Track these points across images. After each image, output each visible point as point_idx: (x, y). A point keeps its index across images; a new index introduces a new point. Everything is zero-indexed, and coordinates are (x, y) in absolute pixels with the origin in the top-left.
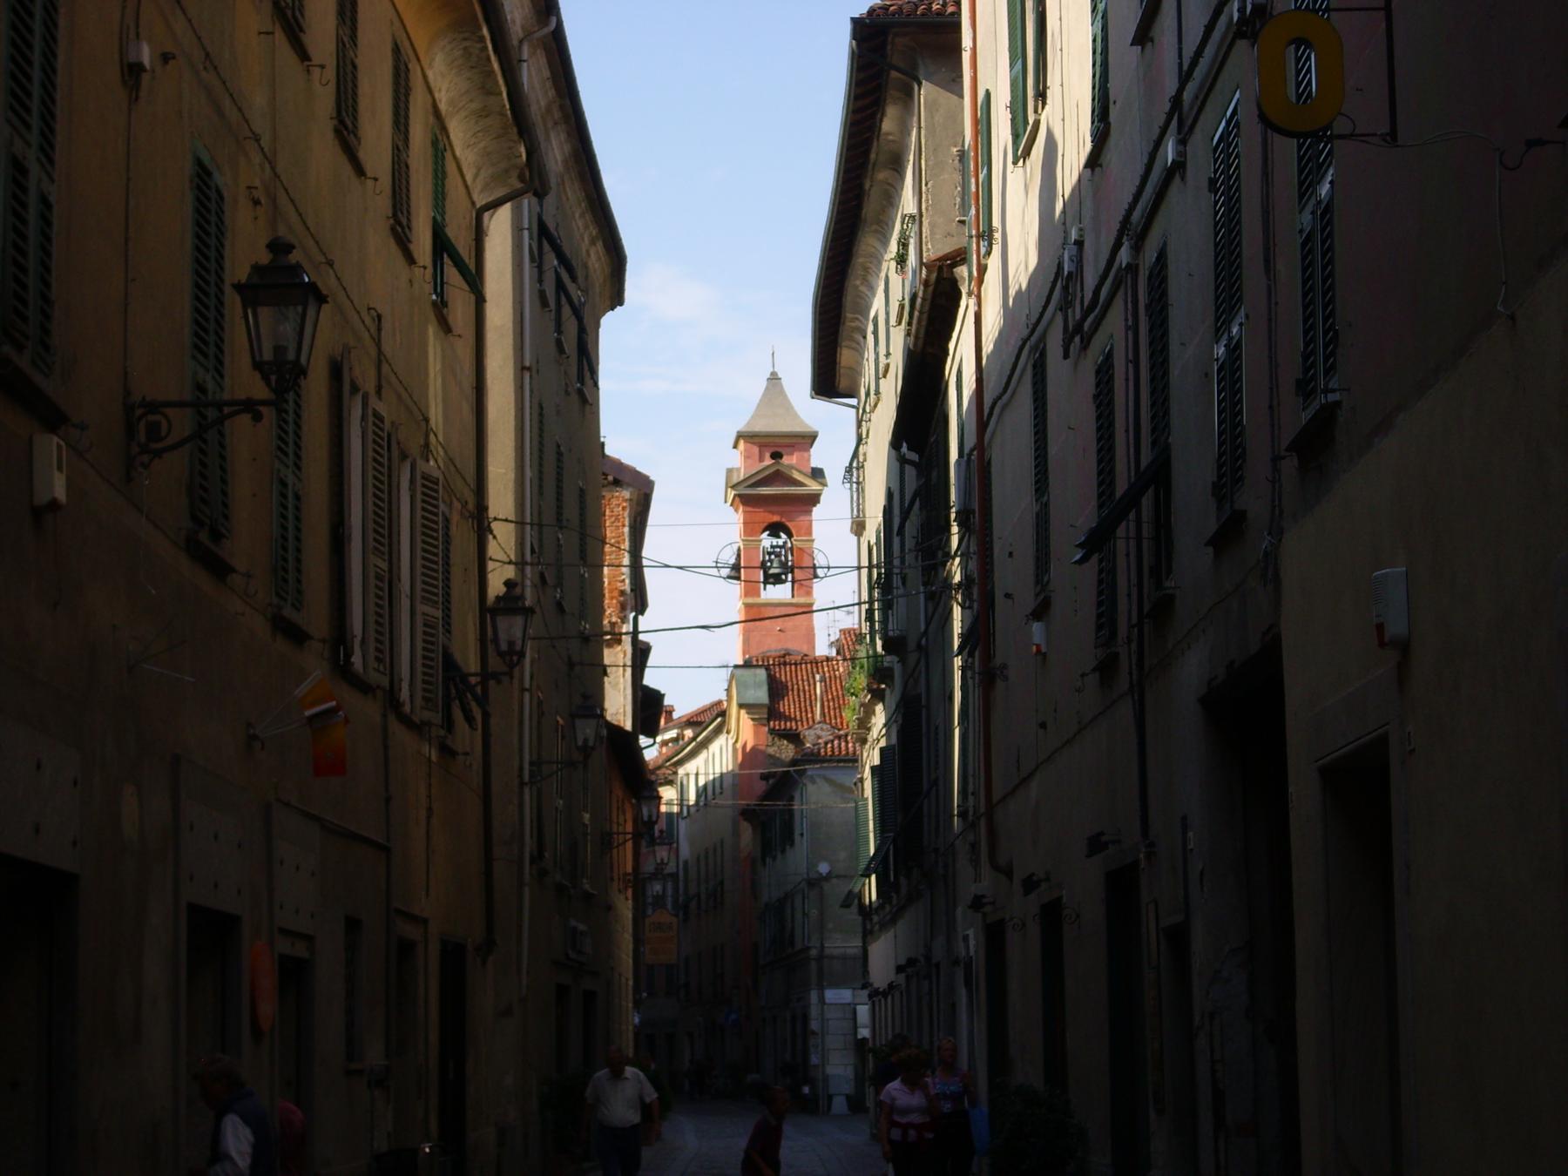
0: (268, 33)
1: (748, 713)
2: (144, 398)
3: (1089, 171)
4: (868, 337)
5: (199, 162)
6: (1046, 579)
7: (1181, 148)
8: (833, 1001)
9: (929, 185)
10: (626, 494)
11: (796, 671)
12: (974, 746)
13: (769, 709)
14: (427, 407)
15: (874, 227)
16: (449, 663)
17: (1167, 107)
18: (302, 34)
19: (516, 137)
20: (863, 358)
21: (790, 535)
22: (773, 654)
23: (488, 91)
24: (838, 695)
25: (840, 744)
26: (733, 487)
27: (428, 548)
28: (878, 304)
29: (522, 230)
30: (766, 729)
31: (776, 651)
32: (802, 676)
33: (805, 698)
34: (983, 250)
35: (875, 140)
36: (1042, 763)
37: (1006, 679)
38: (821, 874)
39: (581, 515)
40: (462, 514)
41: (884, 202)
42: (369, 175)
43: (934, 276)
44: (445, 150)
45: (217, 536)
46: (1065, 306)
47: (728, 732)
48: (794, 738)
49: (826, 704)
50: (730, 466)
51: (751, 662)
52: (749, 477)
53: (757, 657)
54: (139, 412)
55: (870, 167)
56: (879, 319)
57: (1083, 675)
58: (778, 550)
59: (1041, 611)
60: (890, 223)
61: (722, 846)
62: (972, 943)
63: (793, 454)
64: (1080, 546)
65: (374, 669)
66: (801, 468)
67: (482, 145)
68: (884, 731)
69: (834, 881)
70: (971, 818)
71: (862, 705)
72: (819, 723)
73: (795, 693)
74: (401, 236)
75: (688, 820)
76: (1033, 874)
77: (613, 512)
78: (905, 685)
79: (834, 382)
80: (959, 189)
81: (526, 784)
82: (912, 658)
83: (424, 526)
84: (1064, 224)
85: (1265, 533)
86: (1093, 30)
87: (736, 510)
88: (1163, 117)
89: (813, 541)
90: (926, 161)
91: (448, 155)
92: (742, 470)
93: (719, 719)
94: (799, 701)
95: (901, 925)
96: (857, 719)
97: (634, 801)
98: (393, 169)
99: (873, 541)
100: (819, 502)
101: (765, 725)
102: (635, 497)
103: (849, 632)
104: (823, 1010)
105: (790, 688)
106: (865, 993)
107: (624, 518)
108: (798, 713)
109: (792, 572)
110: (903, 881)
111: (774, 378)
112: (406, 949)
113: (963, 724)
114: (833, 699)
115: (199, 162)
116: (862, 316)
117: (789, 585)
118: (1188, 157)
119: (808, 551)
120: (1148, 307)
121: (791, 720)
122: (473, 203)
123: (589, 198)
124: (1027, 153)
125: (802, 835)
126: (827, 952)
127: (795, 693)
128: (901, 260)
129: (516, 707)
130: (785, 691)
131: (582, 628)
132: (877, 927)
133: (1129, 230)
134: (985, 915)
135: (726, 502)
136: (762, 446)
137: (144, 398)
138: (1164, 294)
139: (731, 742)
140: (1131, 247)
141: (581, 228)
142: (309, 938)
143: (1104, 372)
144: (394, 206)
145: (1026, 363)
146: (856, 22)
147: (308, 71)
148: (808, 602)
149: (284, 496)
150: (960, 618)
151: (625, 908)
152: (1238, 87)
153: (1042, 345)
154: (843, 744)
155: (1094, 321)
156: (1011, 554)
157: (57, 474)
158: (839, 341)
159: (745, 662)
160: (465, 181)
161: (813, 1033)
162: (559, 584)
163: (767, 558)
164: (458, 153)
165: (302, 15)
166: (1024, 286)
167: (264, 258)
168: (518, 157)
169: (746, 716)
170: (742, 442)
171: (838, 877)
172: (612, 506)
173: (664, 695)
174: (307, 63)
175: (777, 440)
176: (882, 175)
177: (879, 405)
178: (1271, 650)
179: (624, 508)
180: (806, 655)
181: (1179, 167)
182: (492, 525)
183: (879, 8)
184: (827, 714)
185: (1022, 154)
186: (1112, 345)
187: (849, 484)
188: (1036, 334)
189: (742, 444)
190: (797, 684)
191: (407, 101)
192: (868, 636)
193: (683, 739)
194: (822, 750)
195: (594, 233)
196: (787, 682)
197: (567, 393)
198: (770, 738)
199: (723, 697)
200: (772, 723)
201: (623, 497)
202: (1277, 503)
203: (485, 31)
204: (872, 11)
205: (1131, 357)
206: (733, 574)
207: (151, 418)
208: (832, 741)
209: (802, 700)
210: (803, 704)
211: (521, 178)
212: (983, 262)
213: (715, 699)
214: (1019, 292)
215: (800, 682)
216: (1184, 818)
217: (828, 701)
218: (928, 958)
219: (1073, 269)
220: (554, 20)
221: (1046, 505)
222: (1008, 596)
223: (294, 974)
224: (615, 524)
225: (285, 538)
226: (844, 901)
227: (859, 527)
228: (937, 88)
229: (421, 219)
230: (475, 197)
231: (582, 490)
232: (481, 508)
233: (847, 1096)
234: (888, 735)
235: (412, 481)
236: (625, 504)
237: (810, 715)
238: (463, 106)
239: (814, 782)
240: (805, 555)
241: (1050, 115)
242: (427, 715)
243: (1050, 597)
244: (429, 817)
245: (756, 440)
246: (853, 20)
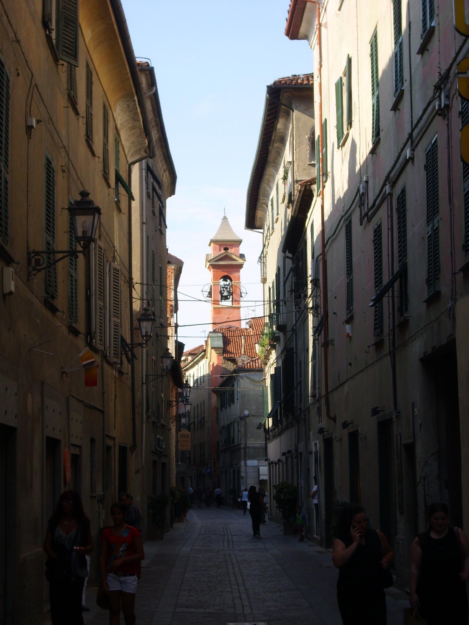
0: (67, 107)
1: (215, 351)
2: (34, 250)
3: (371, 155)
4: (269, 207)
5: (48, 159)
6: (351, 308)
7: (412, 152)
8: (250, 465)
9: (297, 150)
10: (173, 267)
12: (319, 370)
14: (114, 243)
15: (273, 164)
16: (123, 340)
17: (407, 136)
18: (76, 105)
19: (144, 136)
20: (266, 214)
21: (231, 280)
22: (224, 327)
23: (135, 119)
24: (250, 344)
25: (253, 364)
26: (209, 261)
27: (115, 296)
28: (273, 194)
29: (142, 169)
30: (222, 357)
31: (226, 326)
33: (237, 345)
34: (324, 180)
35: (274, 132)
36: (349, 378)
37: (333, 345)
39: (160, 278)
40: (124, 282)
41: (277, 155)
42: (97, 156)
43: (303, 189)
44: (119, 142)
45: (53, 297)
46: (361, 204)
47: (207, 358)
48: (233, 361)
49: (246, 347)
50: (208, 253)
51: (216, 331)
52: (216, 257)
54: (32, 255)
55: (272, 142)
56: (274, 200)
57: (369, 347)
58: (227, 286)
59: (349, 321)
60: (279, 163)
61: (204, 403)
62: (318, 446)
63: (232, 248)
64: (373, 300)
65: (99, 344)
66: (236, 254)
67: (131, 140)
68: (275, 361)
69: (251, 417)
70: (317, 398)
71: (267, 350)
72: (243, 355)
73: (234, 343)
74: (106, 179)
76: (346, 421)
78: (286, 344)
79: (254, 223)
80: (308, 152)
81: (144, 384)
82: (289, 334)
83: (114, 288)
84: (360, 174)
85: (450, 300)
86: (372, 102)
87: (210, 270)
88: (405, 141)
89: (240, 283)
90: (296, 141)
91: (120, 144)
92: (212, 255)
93: (203, 353)
94: (235, 346)
95: (283, 436)
96: (264, 355)
97: (176, 387)
98: (104, 152)
99: (271, 286)
100: (242, 267)
101: (221, 356)
102: (176, 268)
105: (231, 341)
106: (266, 463)
108: (235, 351)
109: (232, 295)
110: (284, 419)
111: (225, 218)
112: (109, 448)
113: (313, 361)
114: (248, 345)
115: (48, 159)
116: (266, 198)
118: (415, 155)
120: (397, 210)
121: (232, 353)
122: (127, 162)
123: (164, 154)
124: (344, 144)
125: (238, 399)
126: (248, 445)
127: (234, 343)
128: (285, 178)
129: (141, 354)
131: (161, 322)
132: (272, 437)
133: (389, 180)
134: (324, 435)
135: (206, 267)
136: (220, 245)
137: (34, 250)
138: (404, 205)
139: (208, 362)
140: (391, 187)
141: (161, 166)
142: (80, 447)
143: (378, 232)
144: (104, 166)
145: (343, 225)
146: (269, 87)
147: (78, 119)
149: (72, 281)
150: (312, 320)
151: (173, 428)
152: (437, 133)
153: (350, 219)
154: (254, 364)
155: (373, 212)
156: (336, 297)
157: (12, 281)
158: (257, 207)
160: (125, 153)
161: (243, 477)
162: (154, 305)
163: (222, 289)
164: (123, 143)
165: (77, 98)
166: (342, 197)
167: (79, 198)
168: (144, 144)
169: (214, 352)
170: (212, 244)
171: (252, 416)
173: (184, 345)
174: (78, 116)
175: (226, 243)
176: (276, 145)
177: (274, 234)
178: (452, 342)
179: (172, 273)
180: (238, 328)
181: (412, 159)
182: (135, 286)
183: (278, 82)
184: (246, 352)
185: (341, 145)
186: (381, 222)
187: (260, 263)
188: (347, 215)
189: (212, 244)
191: (108, 126)
192: (269, 324)
193: (187, 360)
194: (246, 366)
195: (165, 168)
197: (156, 231)
198: (224, 361)
199: (204, 344)
200: (224, 355)
202: (454, 289)
203: (136, 98)
204: (275, 83)
205: (390, 227)
206: (209, 296)
207: (37, 257)
208: (250, 363)
209: (239, 346)
210: (236, 347)
211: (145, 152)
212: (324, 184)
213: (200, 344)
214: (339, 199)
216: (413, 404)
217: (247, 346)
218: (296, 450)
219: (364, 191)
220: (155, 88)
221: (352, 280)
222: (334, 313)
223: (76, 459)
225: (72, 297)
226: (258, 426)
227: (264, 281)
228: (300, 113)
229: (112, 171)
230: (128, 159)
231: (161, 268)
232: (131, 279)
234: (277, 362)
235: (110, 271)
236: (172, 271)
237: (239, 352)
238: (126, 126)
239: (242, 379)
241: (354, 133)
242: (115, 360)
243: (353, 315)
244: (115, 399)
246: (268, 87)
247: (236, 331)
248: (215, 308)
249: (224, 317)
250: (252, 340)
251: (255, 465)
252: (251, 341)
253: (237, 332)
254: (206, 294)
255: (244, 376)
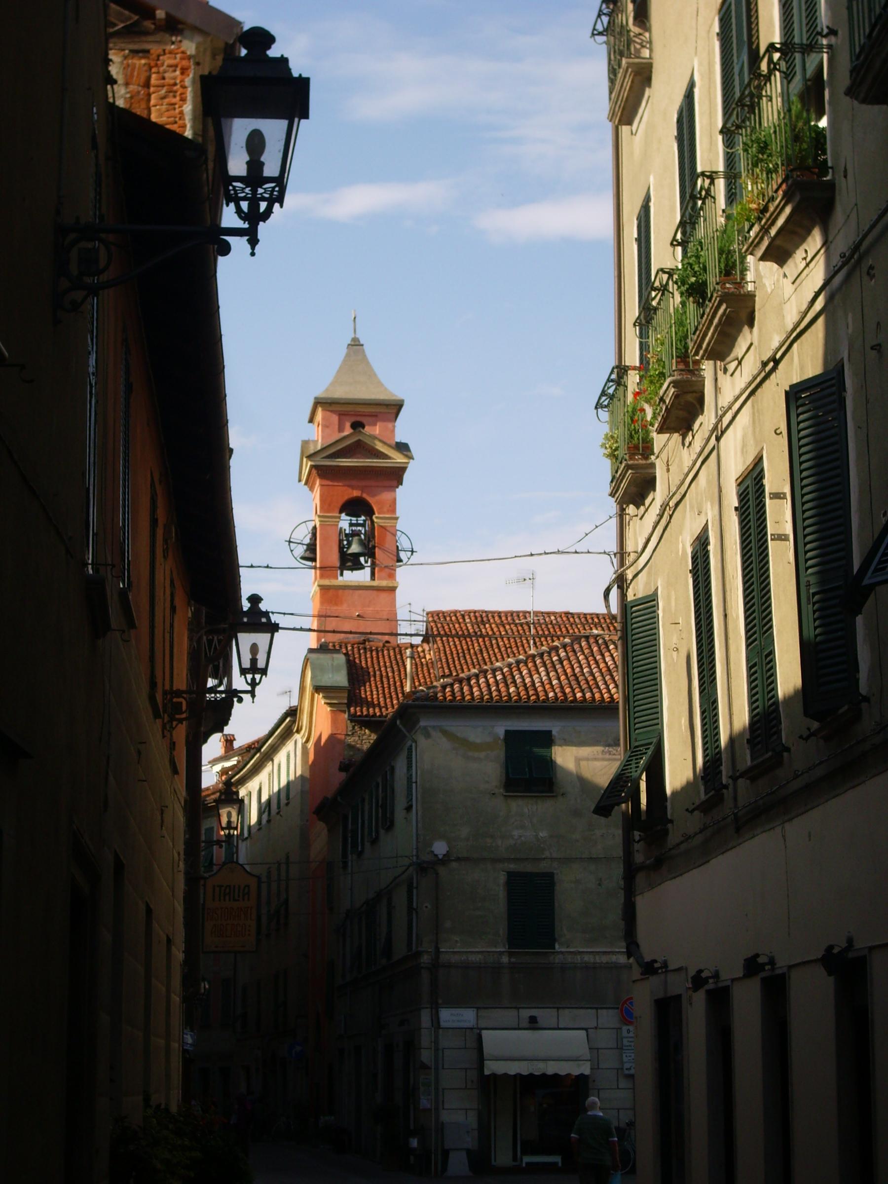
1: (324, 697)
10: (189, 46)
11: (378, 658)
13: (349, 691)
25: (462, 689)
26: (309, 457)
30: (346, 716)
32: (385, 663)
33: (389, 683)
38: (436, 855)
50: (306, 439)
53: (334, 643)
63: (375, 425)
69: (454, 865)
73: (378, 678)
75: (248, 841)
77: (164, 78)
89: (397, 519)
94: (383, 687)
101: (344, 712)
103: (438, 615)
104: (437, 1037)
105: (372, 673)
107: (184, 87)
108: (381, 699)
111: (356, 344)
117: (368, 570)
119: (391, 530)
121: (374, 706)
126: (444, 958)
127: (378, 678)
130: (366, 677)
135: (300, 481)
136: (342, 415)
148: (391, 585)
154: (466, 688)
159: (321, 646)
161: (424, 1067)
169: (323, 701)
171: (458, 859)
172: (161, 69)
190: (380, 670)
196: (368, 668)
200: (352, 709)
201: (183, 52)
208: (452, 685)
209: (392, 688)
210: (386, 691)
215: (383, 669)
224: (166, 101)
233: (469, 1152)
239: (428, 735)
240: (388, 533)
245: (333, 408)
247: (383, 652)
248: (323, 589)
249: (351, 607)
250: (430, 674)
251: (470, 1025)
252: (426, 674)
253: (386, 652)
254: (300, 550)
255: (434, 727)
